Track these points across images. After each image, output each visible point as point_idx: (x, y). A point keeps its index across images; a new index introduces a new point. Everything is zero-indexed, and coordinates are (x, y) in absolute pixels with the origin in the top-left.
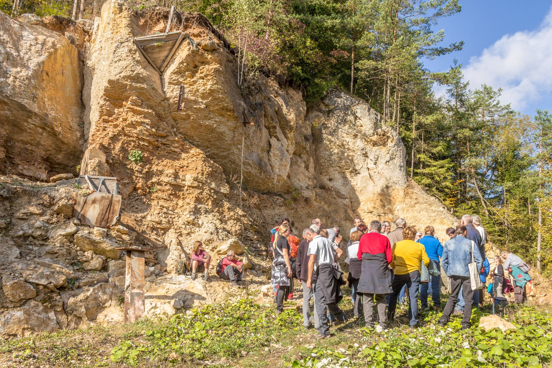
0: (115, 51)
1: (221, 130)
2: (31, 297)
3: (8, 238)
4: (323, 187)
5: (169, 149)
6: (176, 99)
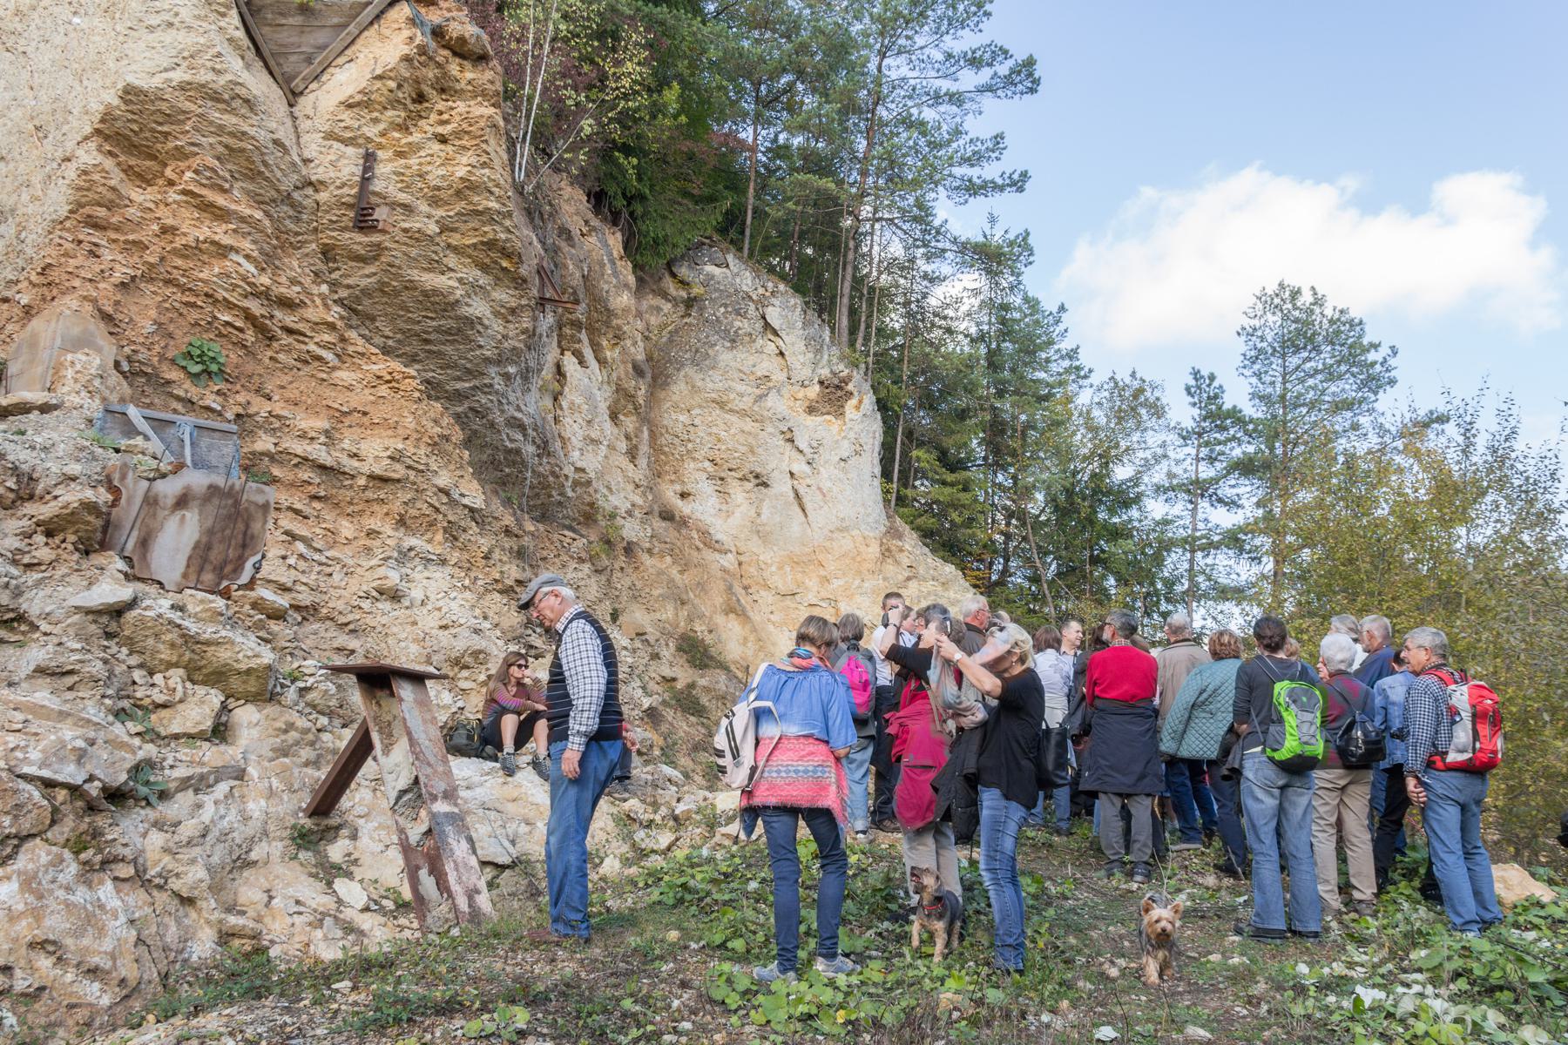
1: (471, 310)
2: (33, 831)
4: (667, 516)
6: (346, 190)
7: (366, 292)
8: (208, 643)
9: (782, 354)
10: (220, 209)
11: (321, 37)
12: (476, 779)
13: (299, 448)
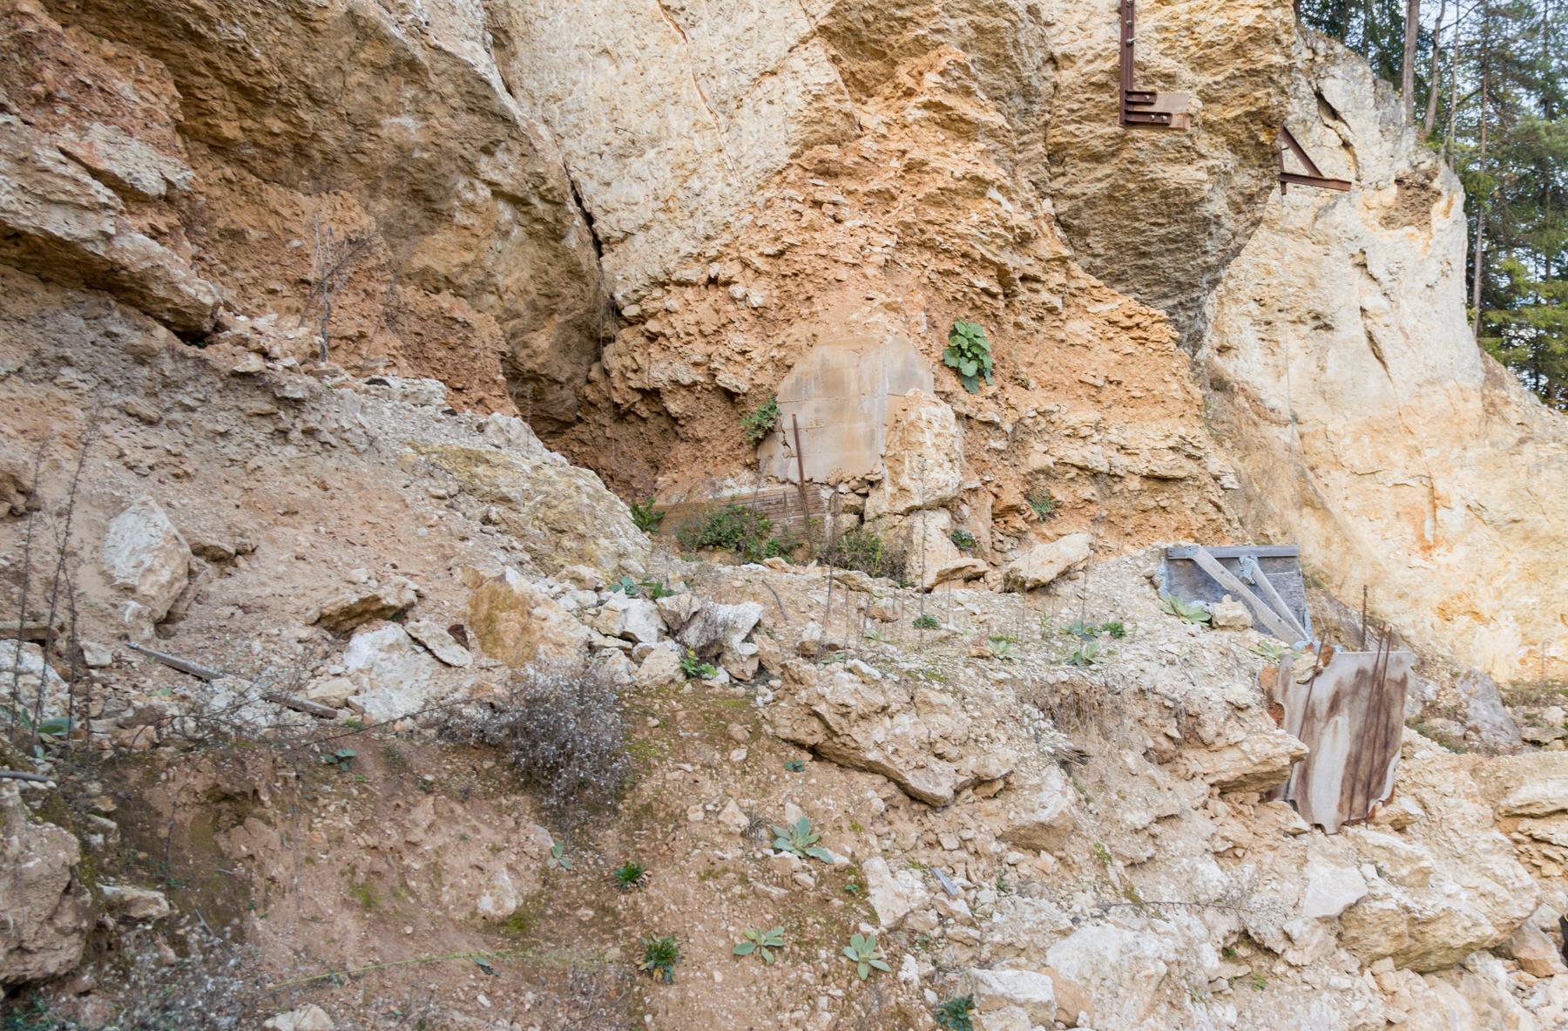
6: (1100, 65)
7: (1091, 203)
9: (1346, 145)
10: (969, 123)
13: (1076, 453)
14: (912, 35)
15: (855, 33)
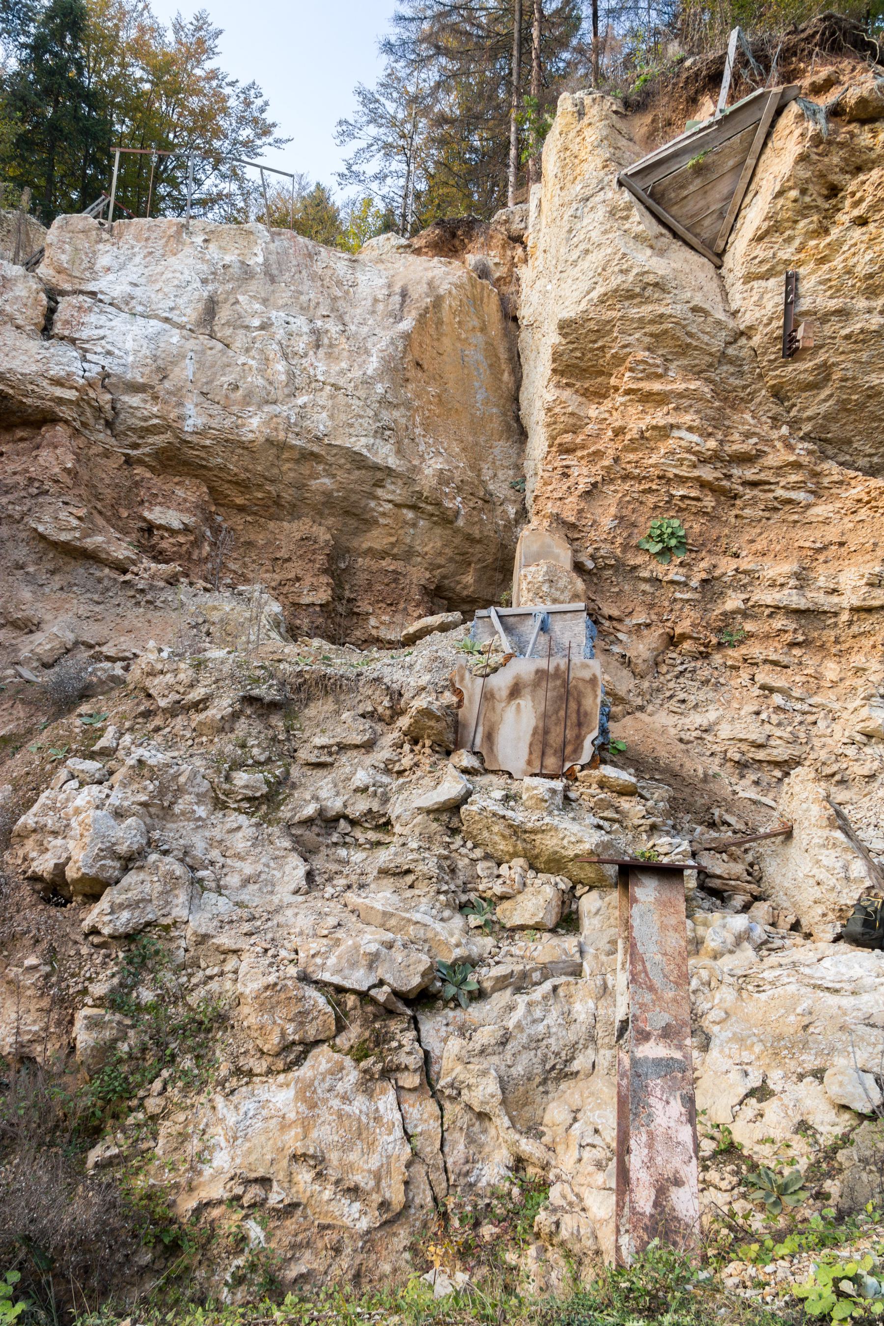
0: (570, 231)
2: (321, 1037)
3: (275, 830)
5: (770, 495)
6: (775, 324)
8: (533, 832)
10: (658, 394)
11: (723, 188)
12: (868, 981)
13: (770, 597)
14: (608, 356)
15: (575, 366)
